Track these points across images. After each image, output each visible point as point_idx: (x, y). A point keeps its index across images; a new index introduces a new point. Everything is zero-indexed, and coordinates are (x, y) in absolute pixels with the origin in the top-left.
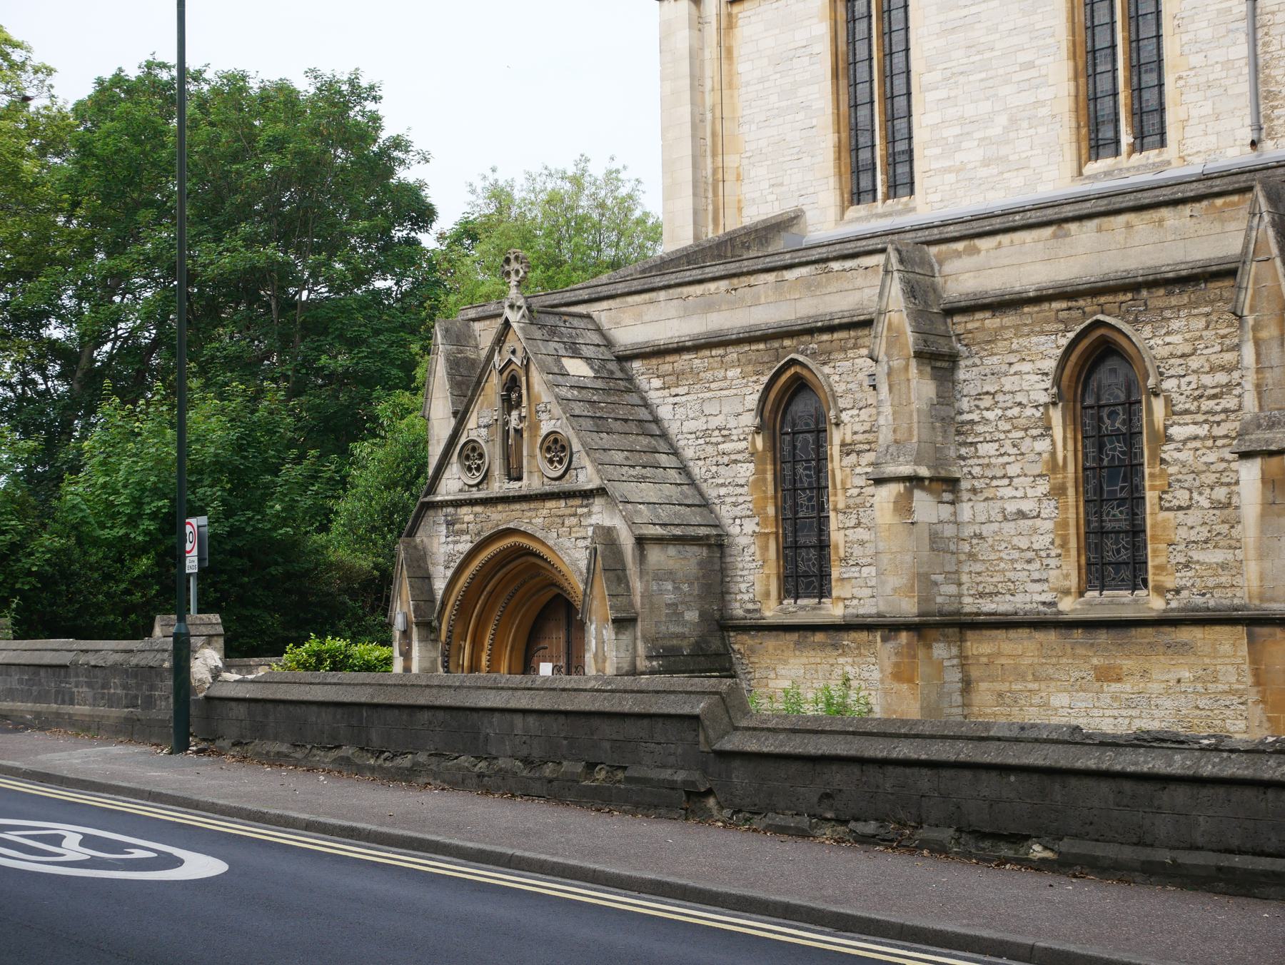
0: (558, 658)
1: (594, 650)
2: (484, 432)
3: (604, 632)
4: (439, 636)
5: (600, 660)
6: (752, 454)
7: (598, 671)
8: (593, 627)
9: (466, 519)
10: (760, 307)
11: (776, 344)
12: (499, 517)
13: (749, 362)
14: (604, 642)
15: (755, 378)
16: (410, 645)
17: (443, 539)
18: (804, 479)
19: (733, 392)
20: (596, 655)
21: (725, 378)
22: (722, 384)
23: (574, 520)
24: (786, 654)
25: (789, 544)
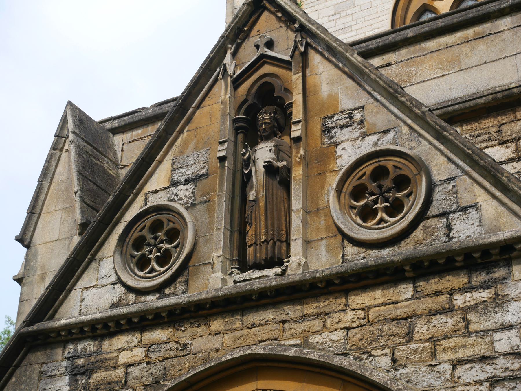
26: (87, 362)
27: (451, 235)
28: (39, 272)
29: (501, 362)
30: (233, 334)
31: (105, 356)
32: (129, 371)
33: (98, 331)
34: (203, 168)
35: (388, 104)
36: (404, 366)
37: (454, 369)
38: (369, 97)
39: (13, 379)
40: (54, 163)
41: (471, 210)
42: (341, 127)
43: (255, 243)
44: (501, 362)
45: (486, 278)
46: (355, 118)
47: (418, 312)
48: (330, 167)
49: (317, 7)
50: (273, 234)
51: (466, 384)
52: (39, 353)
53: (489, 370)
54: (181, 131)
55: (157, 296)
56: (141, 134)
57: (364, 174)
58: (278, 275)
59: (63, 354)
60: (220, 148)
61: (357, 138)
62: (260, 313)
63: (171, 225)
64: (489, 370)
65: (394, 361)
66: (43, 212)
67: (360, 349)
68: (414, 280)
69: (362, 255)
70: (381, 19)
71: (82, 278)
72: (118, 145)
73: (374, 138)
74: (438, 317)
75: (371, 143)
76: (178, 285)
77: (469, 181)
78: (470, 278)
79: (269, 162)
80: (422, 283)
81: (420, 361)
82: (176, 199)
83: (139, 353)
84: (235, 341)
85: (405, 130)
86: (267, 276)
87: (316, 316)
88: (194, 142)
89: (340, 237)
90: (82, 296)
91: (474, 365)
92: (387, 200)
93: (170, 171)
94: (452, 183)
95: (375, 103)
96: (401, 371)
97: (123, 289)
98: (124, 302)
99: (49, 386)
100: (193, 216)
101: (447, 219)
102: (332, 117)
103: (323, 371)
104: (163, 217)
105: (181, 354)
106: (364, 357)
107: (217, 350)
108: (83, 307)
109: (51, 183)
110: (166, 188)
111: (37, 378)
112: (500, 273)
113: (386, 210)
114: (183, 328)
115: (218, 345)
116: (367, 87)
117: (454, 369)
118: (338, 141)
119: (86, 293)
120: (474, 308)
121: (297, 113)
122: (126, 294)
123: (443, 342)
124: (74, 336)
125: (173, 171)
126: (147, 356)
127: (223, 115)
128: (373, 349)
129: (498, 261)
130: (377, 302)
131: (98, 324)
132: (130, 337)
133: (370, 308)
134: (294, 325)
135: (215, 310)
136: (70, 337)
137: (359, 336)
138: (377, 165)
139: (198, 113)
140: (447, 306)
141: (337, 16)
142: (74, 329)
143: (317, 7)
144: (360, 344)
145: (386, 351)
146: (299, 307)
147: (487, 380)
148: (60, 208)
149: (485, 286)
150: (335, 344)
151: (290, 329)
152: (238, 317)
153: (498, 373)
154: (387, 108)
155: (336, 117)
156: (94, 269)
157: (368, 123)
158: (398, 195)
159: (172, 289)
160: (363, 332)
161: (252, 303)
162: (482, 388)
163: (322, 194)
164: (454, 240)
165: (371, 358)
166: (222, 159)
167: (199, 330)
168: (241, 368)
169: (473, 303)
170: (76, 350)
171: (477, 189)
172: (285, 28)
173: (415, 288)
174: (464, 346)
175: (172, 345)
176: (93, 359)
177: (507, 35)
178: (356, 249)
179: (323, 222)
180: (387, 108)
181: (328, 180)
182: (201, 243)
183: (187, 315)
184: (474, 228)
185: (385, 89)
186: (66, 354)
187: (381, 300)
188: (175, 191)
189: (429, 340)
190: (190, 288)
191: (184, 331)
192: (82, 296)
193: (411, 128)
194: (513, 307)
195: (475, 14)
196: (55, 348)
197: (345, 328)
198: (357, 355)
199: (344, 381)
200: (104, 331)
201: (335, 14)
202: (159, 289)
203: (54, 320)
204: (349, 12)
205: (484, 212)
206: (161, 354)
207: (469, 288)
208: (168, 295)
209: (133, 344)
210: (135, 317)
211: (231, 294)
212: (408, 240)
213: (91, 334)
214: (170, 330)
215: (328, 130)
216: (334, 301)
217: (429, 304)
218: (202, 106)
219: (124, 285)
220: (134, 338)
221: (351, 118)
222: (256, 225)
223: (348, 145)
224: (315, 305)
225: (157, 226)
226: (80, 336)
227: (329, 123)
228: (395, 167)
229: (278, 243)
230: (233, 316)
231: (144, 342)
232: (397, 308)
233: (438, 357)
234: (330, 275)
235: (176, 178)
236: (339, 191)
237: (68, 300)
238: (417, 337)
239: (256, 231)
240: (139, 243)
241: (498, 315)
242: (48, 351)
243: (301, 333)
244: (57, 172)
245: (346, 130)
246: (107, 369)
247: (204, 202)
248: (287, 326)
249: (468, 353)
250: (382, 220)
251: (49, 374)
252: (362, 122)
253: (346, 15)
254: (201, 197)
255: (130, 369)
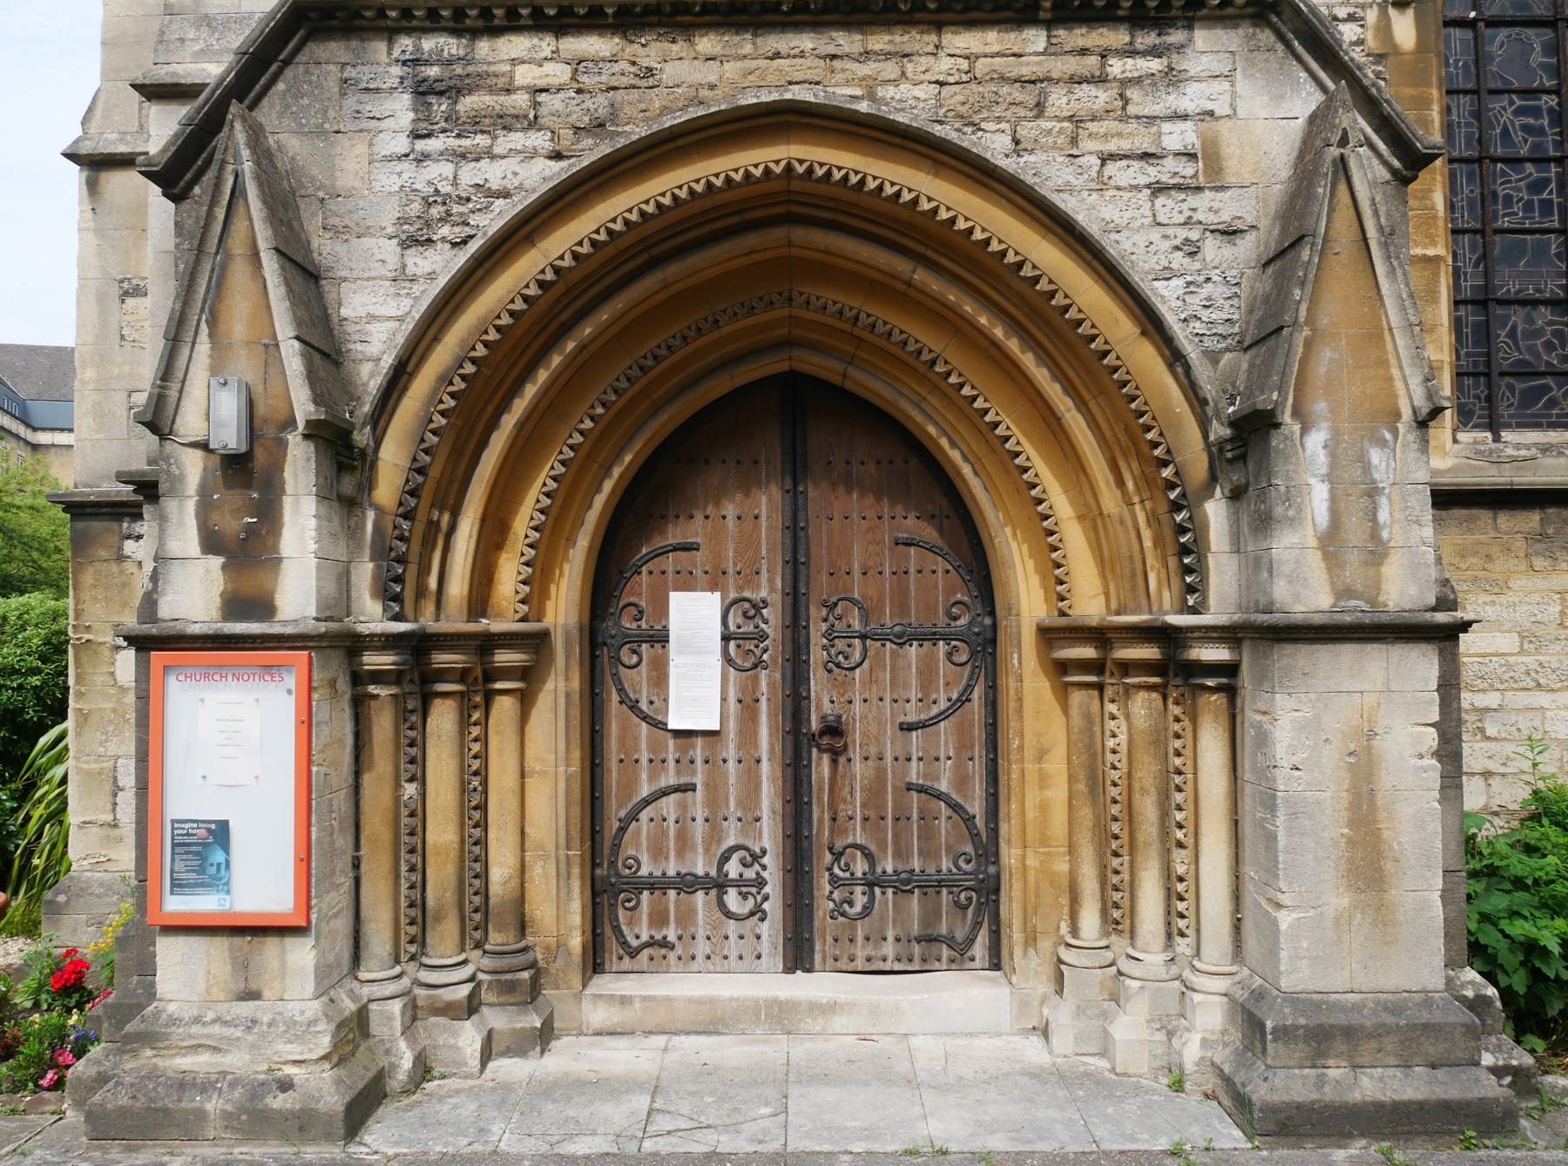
0: (750, 576)
3: (1376, 456)
4: (369, 484)
5: (1353, 558)
8: (1316, 441)
9: (525, 75)
12: (710, 72)
14: (1373, 492)
16: (268, 513)
17: (401, 144)
18: (1518, 136)
23: (1099, 97)
24: (1499, 566)
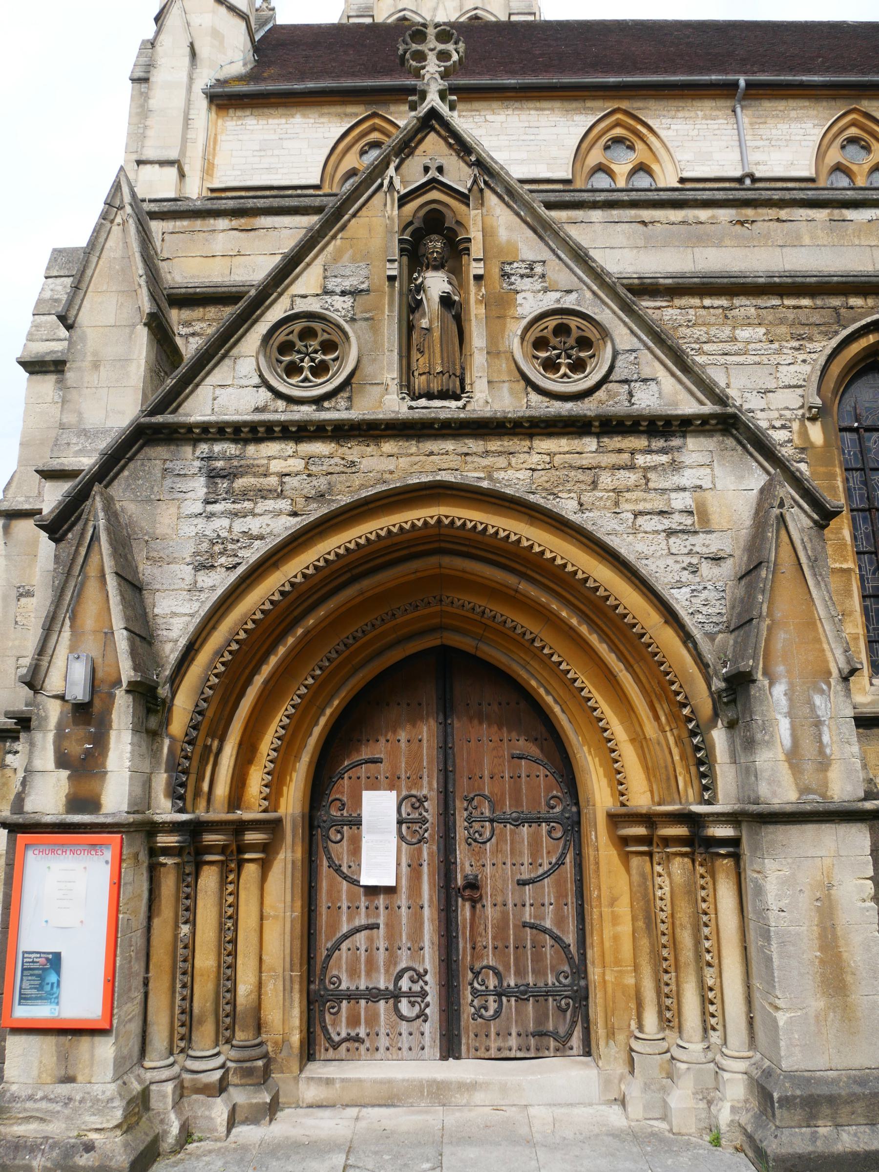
0: (415, 780)
1: (787, 741)
2: (341, 304)
3: (818, 700)
4: (166, 721)
5: (809, 767)
6: (803, 450)
7: (804, 790)
8: (779, 690)
10: (803, 249)
11: (836, 302)
13: (782, 321)
14: (818, 724)
15: (796, 344)
16: (100, 741)
17: (198, 507)
19: (751, 359)
20: (793, 756)
21: (734, 339)
22: (727, 347)
25: (871, 591)
26: (228, 466)
27: (633, 401)
28: (89, 358)
29: (677, 517)
30: (408, 459)
31: (252, 462)
32: (284, 480)
33: (242, 435)
34: (363, 283)
35: (572, 265)
36: (590, 510)
37: (635, 518)
38: (551, 253)
39: (126, 473)
40: (103, 235)
41: (650, 382)
42: (522, 276)
43: (429, 372)
44: (677, 517)
45: (665, 445)
46: (536, 270)
47: (603, 465)
48: (511, 312)
49: (240, 137)
50: (449, 367)
51: (646, 532)
52: (159, 448)
53: (666, 523)
54: (334, 237)
55: (314, 407)
56: (187, 227)
57: (547, 327)
58: (459, 408)
59: (193, 453)
60: (388, 265)
61: (539, 291)
62: (439, 442)
63: (326, 336)
64: (666, 523)
65: (581, 505)
66: (90, 289)
67: (547, 490)
68: (598, 435)
69: (546, 404)
70: (310, 169)
71: (212, 374)
72: (157, 232)
73: (558, 295)
74: (622, 471)
75: (554, 299)
76: (340, 400)
77: (650, 356)
78: (649, 442)
79: (448, 293)
80: (606, 440)
81: (605, 508)
82: (332, 309)
83: (297, 464)
84: (411, 466)
85: (588, 294)
86: (448, 408)
87: (500, 453)
88: (350, 252)
89: (522, 383)
90: (214, 393)
91: (653, 517)
92: (569, 357)
93: (321, 278)
94: (634, 355)
95: (557, 261)
96: (587, 514)
97: (269, 394)
98: (272, 408)
99: (179, 486)
100: (355, 332)
101: (629, 386)
102: (511, 264)
103: (512, 505)
104: (317, 326)
105: (349, 470)
106: (551, 497)
107: (391, 472)
108: (216, 406)
109: (99, 257)
110: (317, 295)
111: (160, 475)
112: (676, 442)
113: (569, 366)
114: (349, 445)
115: (392, 468)
116: (551, 243)
117: (635, 518)
118: (518, 289)
119: (218, 391)
120: (654, 468)
121: (476, 249)
122: (274, 400)
123: (625, 494)
124: (210, 436)
125: (325, 278)
126: (306, 468)
127: (389, 231)
128: (560, 491)
129: (676, 431)
130: (561, 450)
131: (245, 427)
132: (283, 446)
133: (555, 454)
134: (477, 459)
135: (389, 432)
136: (204, 436)
137: (545, 478)
138: (560, 321)
139: (353, 221)
140: (629, 464)
141: (262, 153)
142: (212, 428)
143: (240, 137)
144: (547, 485)
145: (572, 495)
146: (481, 443)
147: (664, 531)
148: (114, 289)
149: (663, 451)
150: (521, 483)
151: (473, 462)
152: (414, 442)
153: (674, 526)
154: (571, 269)
155: (515, 265)
156: (229, 366)
157: (549, 278)
158: (582, 354)
159: (333, 404)
160: (549, 475)
161: (433, 432)
162: (659, 537)
163: (503, 338)
164: (635, 406)
165: (558, 500)
166: (392, 279)
167: (369, 449)
168: (424, 492)
169: (653, 464)
170: (211, 451)
171: (657, 364)
172: (456, 158)
173: (598, 442)
174: (645, 500)
175: (337, 460)
176: (236, 463)
177: (598, 227)
178: (540, 398)
179: (504, 365)
180: (571, 269)
181: (508, 325)
182: (365, 361)
183: (357, 433)
184: (654, 399)
185: (574, 250)
186: (198, 453)
187: (566, 449)
188: (329, 301)
189: (614, 490)
190: (354, 405)
191: (349, 448)
192: (214, 393)
193: (594, 293)
194: (687, 472)
195: (572, 199)
196: (182, 445)
197: (530, 469)
198: (543, 495)
199: (531, 516)
200: (250, 436)
201: (260, 150)
202: (318, 401)
203: (177, 414)
204: (276, 152)
205: (663, 386)
206: (324, 468)
207: (650, 452)
208: (328, 409)
209: (287, 454)
210: (293, 426)
211: (413, 419)
212: (591, 399)
213: (232, 436)
214: (333, 445)
215: (509, 276)
216: (518, 442)
217: (613, 459)
218: (358, 215)
219: (271, 389)
220: (289, 447)
221: (532, 269)
222: (430, 355)
223: (528, 295)
224: (499, 443)
225: (307, 334)
226: (218, 436)
227: (507, 268)
228: (578, 327)
229: (453, 377)
230: (407, 441)
231: (301, 454)
232: (582, 458)
233: (621, 506)
234: (522, 417)
235: (330, 287)
236: (523, 338)
237: (194, 394)
238: (601, 486)
239: (429, 360)
240: (286, 348)
241: (675, 478)
242: (173, 448)
243: (485, 467)
244: (107, 246)
245: (526, 280)
246: (255, 475)
247: (367, 319)
248: (468, 458)
249: (648, 506)
250: (565, 375)
251: (177, 472)
252: (543, 276)
253: (272, 155)
254: (362, 312)
255: (286, 479)
